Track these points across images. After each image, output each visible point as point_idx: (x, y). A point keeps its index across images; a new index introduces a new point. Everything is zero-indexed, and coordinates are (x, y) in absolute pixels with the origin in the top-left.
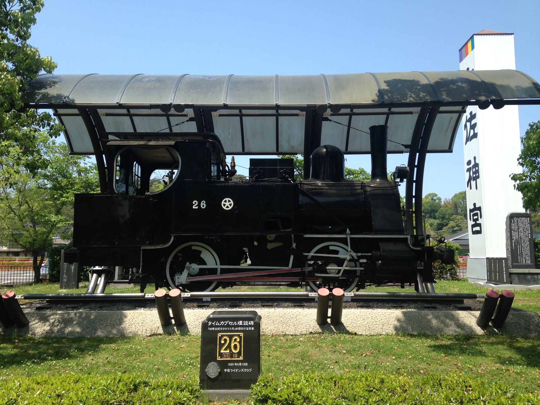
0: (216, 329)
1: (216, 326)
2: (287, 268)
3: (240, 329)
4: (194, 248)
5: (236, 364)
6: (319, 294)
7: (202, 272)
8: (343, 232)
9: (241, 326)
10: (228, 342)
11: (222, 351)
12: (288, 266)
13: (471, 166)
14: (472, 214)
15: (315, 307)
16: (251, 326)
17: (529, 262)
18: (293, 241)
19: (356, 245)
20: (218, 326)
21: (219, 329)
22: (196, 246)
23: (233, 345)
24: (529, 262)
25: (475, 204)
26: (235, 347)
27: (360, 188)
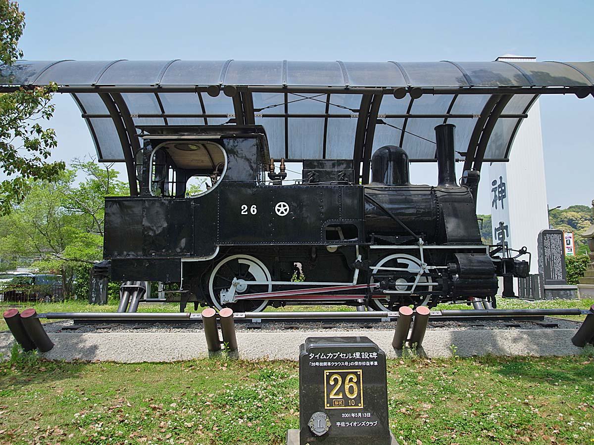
0: (321, 364)
1: (320, 360)
2: (351, 284)
3: (356, 363)
4: (240, 261)
5: (353, 415)
6: (400, 314)
7: (251, 289)
8: (415, 242)
9: (358, 360)
10: (340, 383)
11: (331, 397)
12: (352, 282)
13: (497, 186)
14: (497, 233)
16: (373, 360)
17: (561, 278)
18: (358, 253)
19: (430, 257)
20: (324, 360)
21: (325, 364)
22: (243, 259)
23: (347, 387)
24: (561, 278)
25: (501, 224)
26: (351, 390)
27: (429, 192)
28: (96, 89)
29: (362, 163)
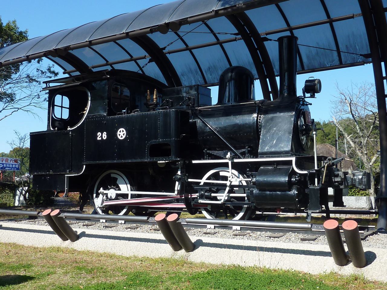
15: (370, 62)
19: (241, 168)
28: (127, 35)
29: (268, 79)
